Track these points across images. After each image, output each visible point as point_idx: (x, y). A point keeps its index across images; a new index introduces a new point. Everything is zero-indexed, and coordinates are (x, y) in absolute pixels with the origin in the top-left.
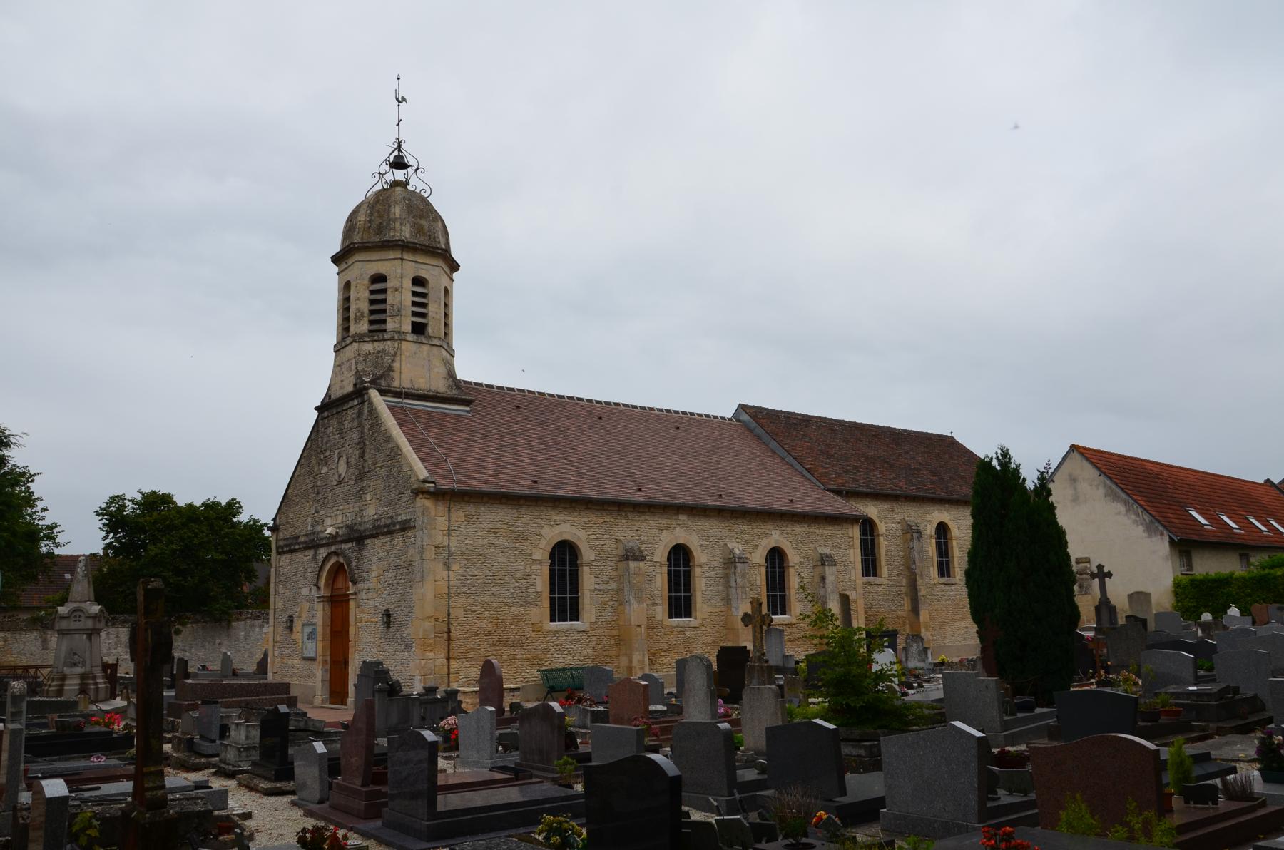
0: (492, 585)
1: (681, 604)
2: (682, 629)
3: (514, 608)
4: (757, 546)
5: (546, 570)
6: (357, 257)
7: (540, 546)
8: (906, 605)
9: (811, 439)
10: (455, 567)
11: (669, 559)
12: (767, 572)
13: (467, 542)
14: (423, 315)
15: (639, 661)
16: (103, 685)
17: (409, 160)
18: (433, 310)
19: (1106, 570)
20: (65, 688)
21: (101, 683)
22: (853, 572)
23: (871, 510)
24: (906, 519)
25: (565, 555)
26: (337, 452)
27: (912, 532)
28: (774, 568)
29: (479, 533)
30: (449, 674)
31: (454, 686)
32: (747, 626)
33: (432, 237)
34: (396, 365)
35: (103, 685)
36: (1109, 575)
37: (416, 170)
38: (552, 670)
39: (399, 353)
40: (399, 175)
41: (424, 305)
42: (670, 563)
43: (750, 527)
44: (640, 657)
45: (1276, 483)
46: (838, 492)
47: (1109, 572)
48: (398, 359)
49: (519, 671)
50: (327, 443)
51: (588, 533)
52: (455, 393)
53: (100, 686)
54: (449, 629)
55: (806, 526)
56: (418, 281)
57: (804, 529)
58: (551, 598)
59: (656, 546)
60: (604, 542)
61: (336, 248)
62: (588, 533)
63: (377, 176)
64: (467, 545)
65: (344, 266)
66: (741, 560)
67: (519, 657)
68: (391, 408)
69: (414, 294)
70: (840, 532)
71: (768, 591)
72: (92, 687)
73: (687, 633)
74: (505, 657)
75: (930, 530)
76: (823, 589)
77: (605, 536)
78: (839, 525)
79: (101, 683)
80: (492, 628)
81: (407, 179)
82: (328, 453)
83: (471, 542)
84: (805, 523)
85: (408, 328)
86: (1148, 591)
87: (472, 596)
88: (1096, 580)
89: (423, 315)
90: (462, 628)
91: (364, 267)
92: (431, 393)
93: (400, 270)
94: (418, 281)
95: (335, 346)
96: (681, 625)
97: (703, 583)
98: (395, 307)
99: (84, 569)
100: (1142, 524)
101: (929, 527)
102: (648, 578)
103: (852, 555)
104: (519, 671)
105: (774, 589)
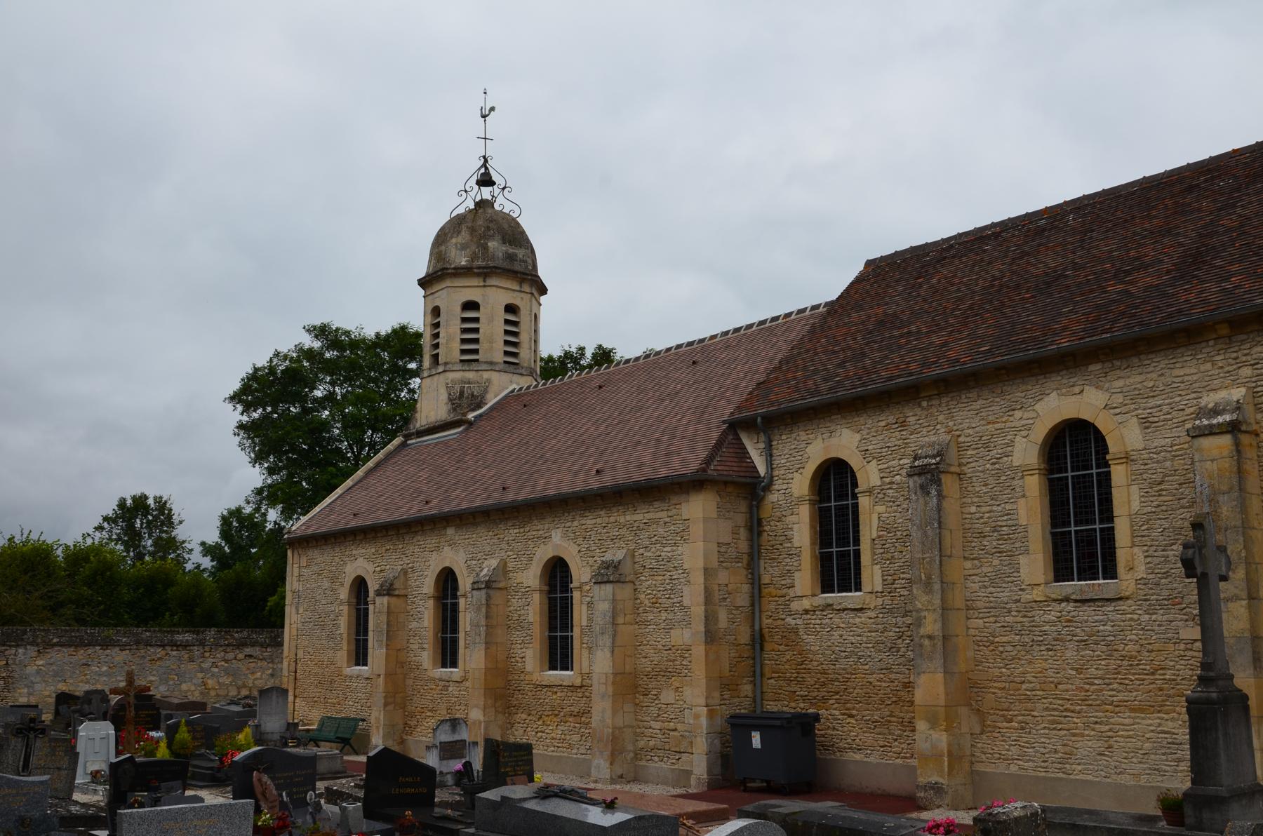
2: (447, 684)
6: (448, 283)
17: (495, 177)
37: (504, 189)
40: (486, 193)
43: (522, 530)
55: (602, 513)
57: (599, 521)
61: (422, 274)
63: (463, 193)
70: (664, 514)
73: (450, 689)
78: (663, 500)
81: (493, 196)
84: (602, 510)
91: (453, 296)
93: (494, 297)
94: (511, 309)
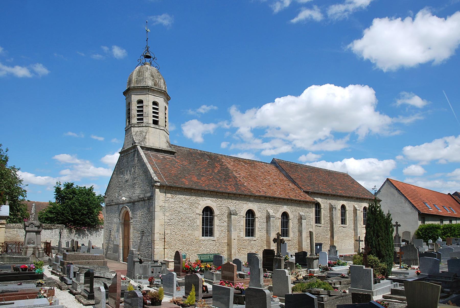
0: (181, 222)
1: (250, 232)
3: (189, 231)
4: (278, 211)
5: (201, 217)
7: (199, 208)
8: (329, 234)
9: (298, 172)
10: (167, 214)
11: (246, 215)
12: (281, 221)
13: (172, 205)
14: (157, 117)
15: (234, 252)
16: (42, 252)
18: (161, 115)
19: (398, 224)
20: (27, 252)
21: (41, 251)
22: (312, 221)
23: (319, 200)
24: (331, 203)
25: (208, 211)
26: (126, 169)
27: (332, 208)
28: (284, 219)
29: (176, 202)
30: (164, 254)
31: (166, 259)
32: (274, 243)
33: (160, 85)
34: (147, 137)
35: (42, 252)
36: (400, 225)
38: (203, 254)
39: (148, 132)
41: (157, 113)
42: (247, 216)
44: (234, 251)
45: (451, 194)
46: (307, 193)
47: (400, 224)
48: (148, 134)
49: (190, 254)
50: (123, 166)
51: (217, 204)
52: (169, 149)
53: (40, 252)
54: (165, 238)
56: (155, 103)
58: (203, 228)
59: (242, 210)
60: (222, 208)
62: (217, 204)
64: (171, 206)
65: (127, 96)
66: (272, 216)
67: (190, 249)
68: (145, 154)
69: (154, 108)
71: (281, 228)
72: (37, 252)
74: (185, 249)
75: (339, 207)
76: (301, 228)
77: (223, 205)
79: (41, 251)
80: (180, 238)
82: (123, 170)
83: (173, 206)
85: (151, 122)
86: (410, 231)
87: (173, 226)
88: (395, 227)
89: (157, 117)
90: (169, 237)
92: (160, 149)
94: (155, 103)
95: (125, 128)
96: (250, 239)
97: (259, 224)
98: (146, 113)
99: (34, 208)
100: (409, 207)
101: (339, 206)
102: (238, 221)
103: (312, 216)
104: (190, 254)
105: (284, 227)
